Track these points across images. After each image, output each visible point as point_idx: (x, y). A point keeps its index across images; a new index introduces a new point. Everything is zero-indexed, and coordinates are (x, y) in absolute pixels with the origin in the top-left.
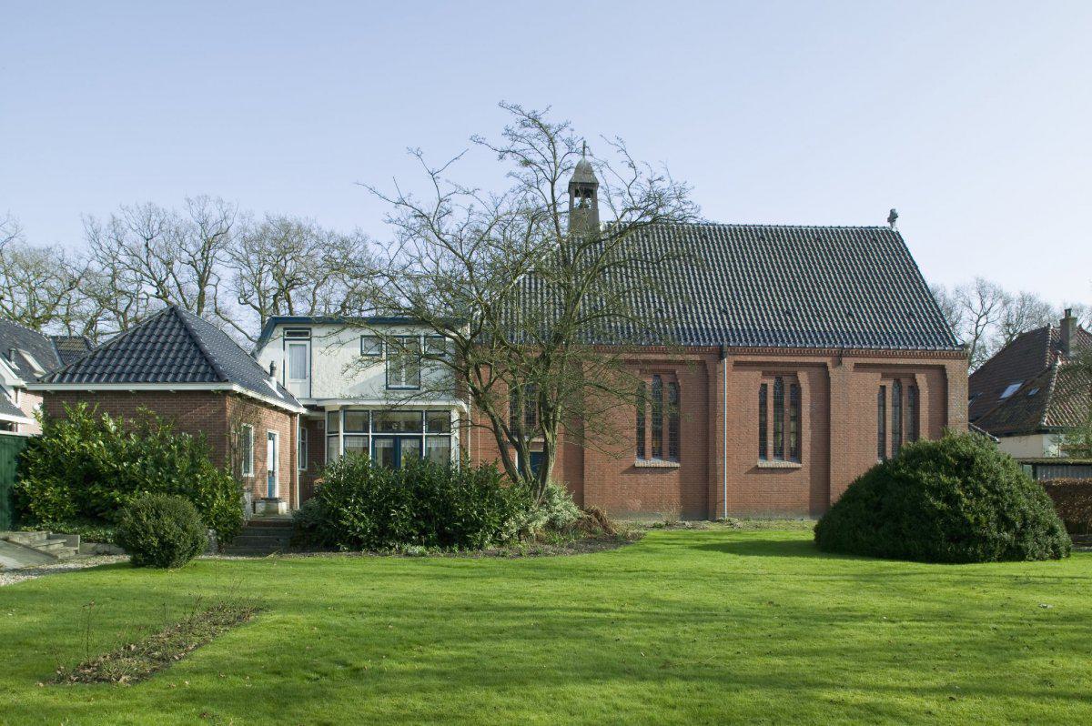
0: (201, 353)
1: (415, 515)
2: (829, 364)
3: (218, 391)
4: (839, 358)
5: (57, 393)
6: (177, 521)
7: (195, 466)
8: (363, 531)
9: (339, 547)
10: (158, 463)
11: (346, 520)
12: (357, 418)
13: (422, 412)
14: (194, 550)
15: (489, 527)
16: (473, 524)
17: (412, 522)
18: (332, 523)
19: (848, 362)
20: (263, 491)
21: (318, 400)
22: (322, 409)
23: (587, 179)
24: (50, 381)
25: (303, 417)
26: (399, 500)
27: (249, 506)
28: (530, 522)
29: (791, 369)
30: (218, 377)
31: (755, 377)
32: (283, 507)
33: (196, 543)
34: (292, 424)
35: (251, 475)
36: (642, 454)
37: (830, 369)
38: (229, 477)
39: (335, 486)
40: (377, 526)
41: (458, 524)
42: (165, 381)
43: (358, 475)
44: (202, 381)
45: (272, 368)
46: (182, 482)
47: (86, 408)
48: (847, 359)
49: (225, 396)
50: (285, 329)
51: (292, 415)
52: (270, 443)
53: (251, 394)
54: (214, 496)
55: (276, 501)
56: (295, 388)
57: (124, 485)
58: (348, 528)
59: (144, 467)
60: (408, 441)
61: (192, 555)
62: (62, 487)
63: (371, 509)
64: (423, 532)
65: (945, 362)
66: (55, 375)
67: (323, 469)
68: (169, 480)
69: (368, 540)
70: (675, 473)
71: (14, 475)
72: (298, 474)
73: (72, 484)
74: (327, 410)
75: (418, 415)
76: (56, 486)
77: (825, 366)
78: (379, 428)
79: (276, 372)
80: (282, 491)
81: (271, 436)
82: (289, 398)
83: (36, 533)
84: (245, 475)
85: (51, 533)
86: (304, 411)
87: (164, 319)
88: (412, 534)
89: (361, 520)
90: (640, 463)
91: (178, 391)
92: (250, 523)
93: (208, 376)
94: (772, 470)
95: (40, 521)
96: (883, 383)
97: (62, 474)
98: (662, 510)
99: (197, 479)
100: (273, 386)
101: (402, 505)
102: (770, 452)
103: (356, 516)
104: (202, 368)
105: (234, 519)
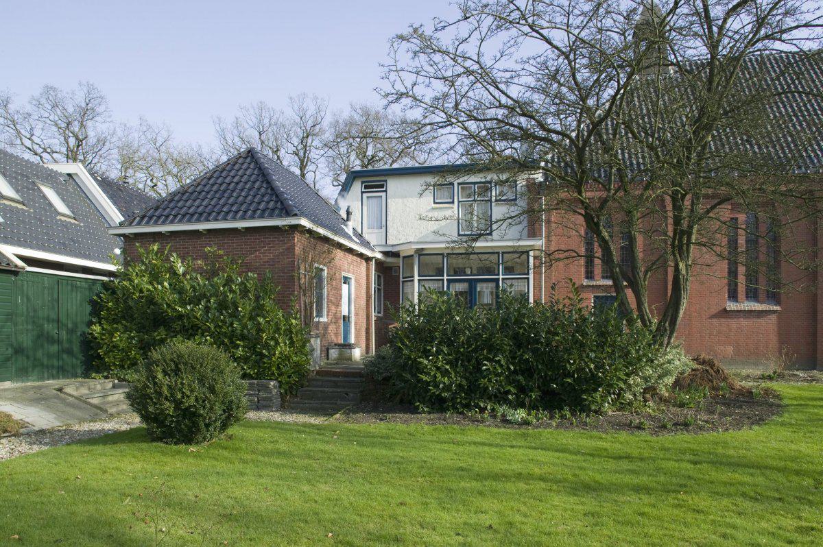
0: (272, 189)
1: (512, 368)
3: (284, 226)
5: (136, 235)
6: (201, 381)
7: (259, 309)
8: (447, 388)
9: (417, 408)
10: (222, 306)
11: (427, 374)
12: (429, 261)
13: (498, 253)
14: (228, 418)
15: (610, 386)
16: (587, 381)
17: (507, 377)
18: (409, 376)
20: (336, 335)
21: (393, 246)
22: (396, 255)
24: (130, 224)
25: (378, 263)
26: (493, 348)
27: (317, 353)
28: (660, 377)
30: (287, 211)
32: (357, 354)
33: (229, 409)
34: (368, 269)
35: (324, 319)
36: (733, 296)
38: (293, 321)
39: (414, 331)
40: (464, 382)
41: (569, 380)
42: (234, 218)
43: (441, 317)
44: (271, 216)
45: (348, 213)
46: (245, 326)
47: (158, 249)
49: (293, 232)
50: (362, 183)
51: (368, 259)
52: (345, 287)
53: (322, 231)
54: (277, 343)
55: (350, 346)
56: (372, 236)
57: (187, 330)
58: (428, 383)
59: (207, 309)
60: (485, 285)
61: (224, 426)
62: (131, 332)
63: (457, 360)
64: (522, 390)
66: (135, 218)
67: (397, 310)
68: (232, 324)
69: (453, 399)
70: (774, 317)
71: (87, 320)
72: (374, 319)
73: (141, 329)
74: (402, 255)
75: (493, 258)
76: (125, 332)
78: (452, 273)
79: (352, 217)
80: (357, 336)
81: (346, 280)
82: (366, 244)
83: (103, 381)
84: (316, 319)
85: (116, 381)
86: (379, 256)
87: (241, 161)
88: (508, 392)
89: (445, 373)
90: (732, 306)
91: (247, 229)
92: (318, 373)
93: (277, 212)
94: (750, 313)
95: (108, 368)
97: (132, 318)
98: (767, 359)
99: (259, 324)
100: (350, 232)
101: (496, 356)
103: (438, 369)
104: (271, 205)
105: (299, 369)
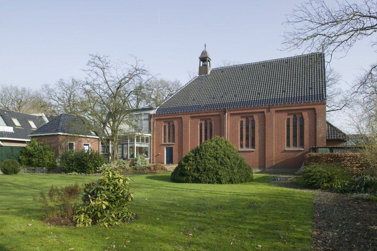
2: (265, 112)
4: (269, 109)
19: (273, 110)
23: (205, 56)
29: (299, 112)
31: (285, 116)
37: (266, 113)
48: (272, 109)
65: (182, 116)
77: (263, 112)
94: (244, 152)
96: (289, 117)
102: (291, 143)
